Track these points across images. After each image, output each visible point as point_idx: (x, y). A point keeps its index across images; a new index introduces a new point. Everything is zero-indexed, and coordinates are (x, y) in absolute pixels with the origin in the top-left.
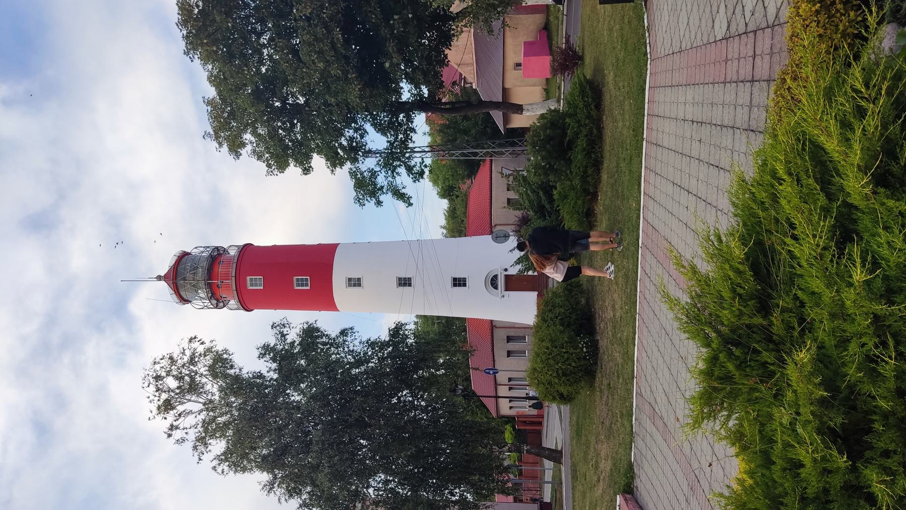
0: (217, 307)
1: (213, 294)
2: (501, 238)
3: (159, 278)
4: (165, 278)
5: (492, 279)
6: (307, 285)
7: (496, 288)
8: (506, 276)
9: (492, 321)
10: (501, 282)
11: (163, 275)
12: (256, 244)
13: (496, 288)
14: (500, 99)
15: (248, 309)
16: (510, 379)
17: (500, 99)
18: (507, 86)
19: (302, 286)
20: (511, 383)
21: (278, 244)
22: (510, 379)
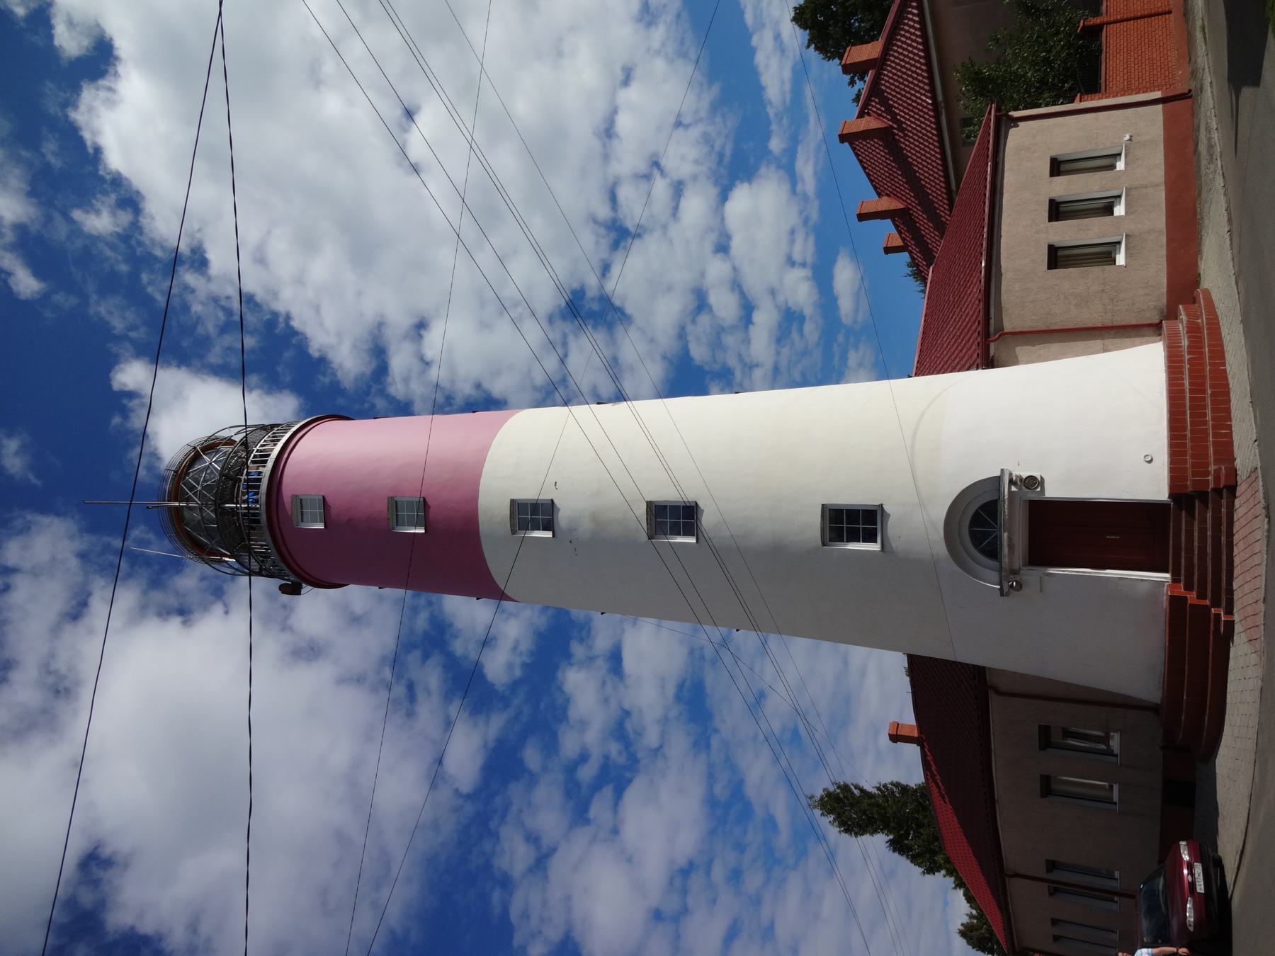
2: (533, 514)
5: (977, 520)
7: (992, 552)
10: (1014, 535)
13: (992, 552)
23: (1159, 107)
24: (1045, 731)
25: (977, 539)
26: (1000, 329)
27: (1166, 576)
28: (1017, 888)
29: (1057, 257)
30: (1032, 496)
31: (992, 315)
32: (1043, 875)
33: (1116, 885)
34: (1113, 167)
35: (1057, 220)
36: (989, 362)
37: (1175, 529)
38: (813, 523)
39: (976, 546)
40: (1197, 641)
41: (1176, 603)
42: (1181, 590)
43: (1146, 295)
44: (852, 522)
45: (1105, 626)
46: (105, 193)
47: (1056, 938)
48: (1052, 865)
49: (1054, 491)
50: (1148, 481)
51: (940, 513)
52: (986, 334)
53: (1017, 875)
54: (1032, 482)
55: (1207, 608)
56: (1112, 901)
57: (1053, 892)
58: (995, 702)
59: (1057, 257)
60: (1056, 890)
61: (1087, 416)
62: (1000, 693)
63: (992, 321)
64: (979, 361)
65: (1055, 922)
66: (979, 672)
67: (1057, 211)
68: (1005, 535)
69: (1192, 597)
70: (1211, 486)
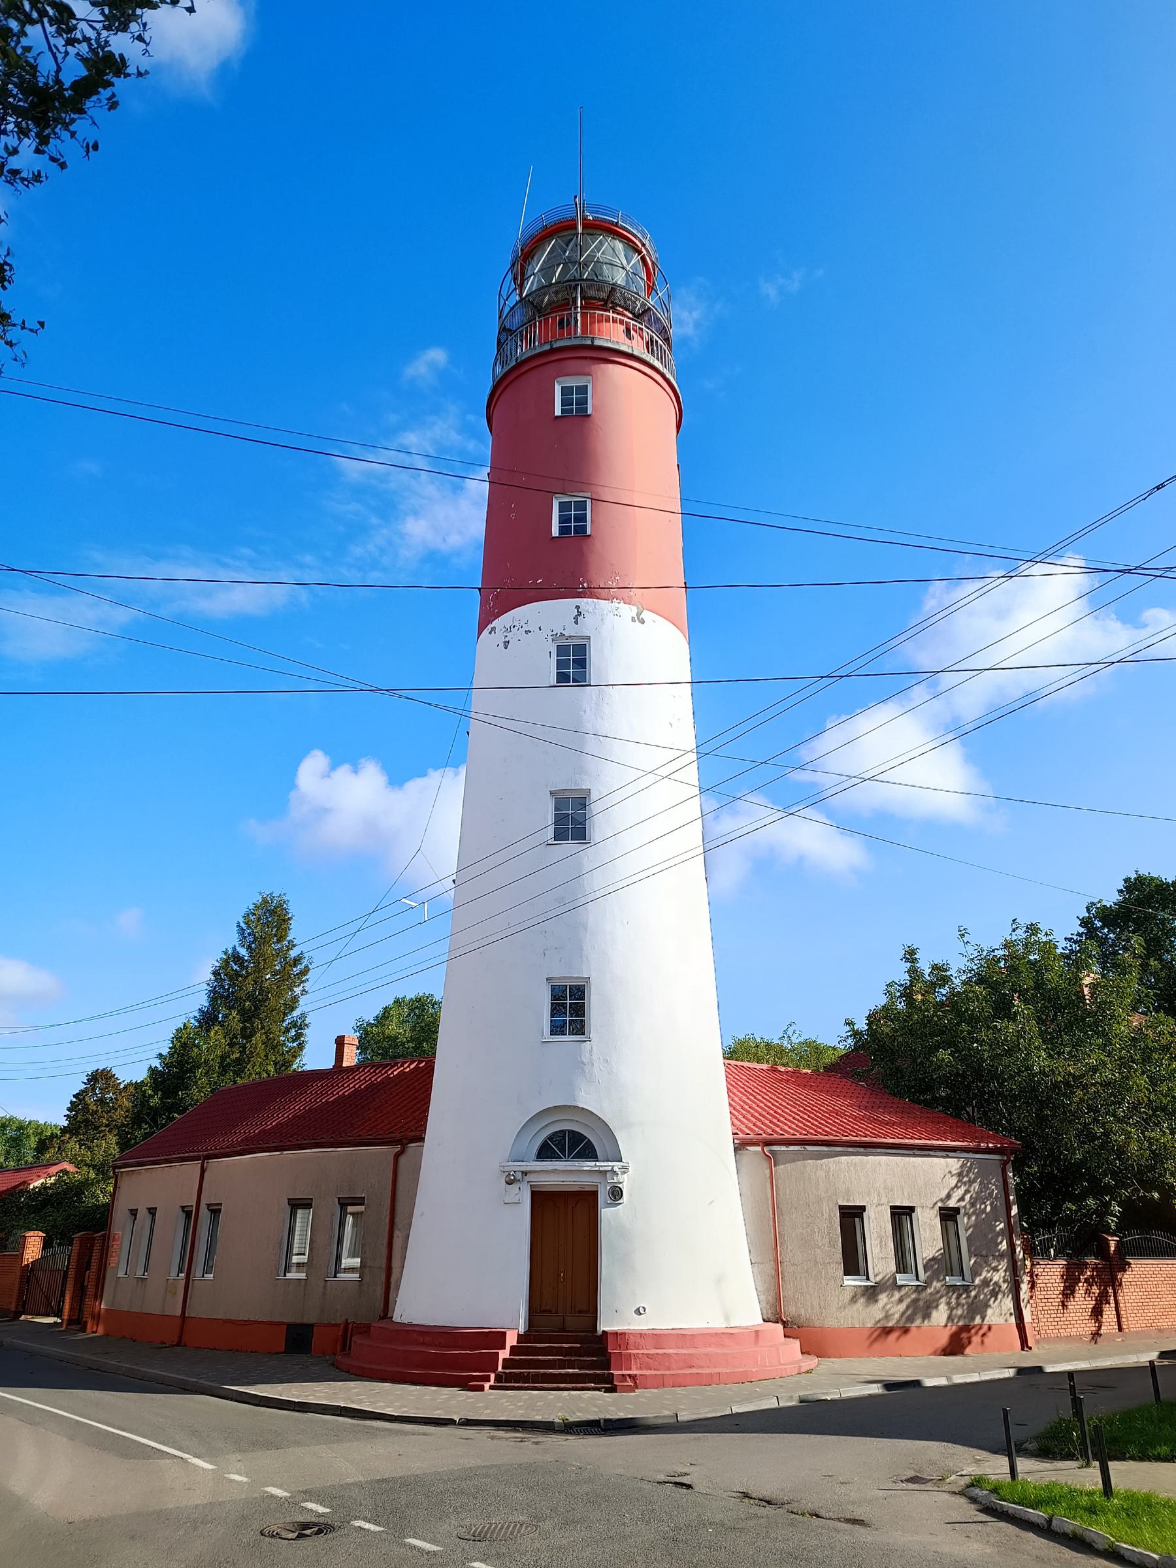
7: (545, 1152)
10: (564, 1174)
13: (545, 1152)
29: (851, 1216)
30: (603, 1197)
31: (792, 1148)
35: (892, 1214)
36: (740, 1146)
37: (568, 1335)
39: (551, 1137)
40: (453, 1357)
43: (812, 1307)
44: (570, 1008)
45: (464, 1262)
47: (134, 1213)
48: (215, 1211)
51: (585, 1100)
53: (203, 1171)
55: (495, 1370)
57: (188, 1214)
60: (188, 1215)
61: (692, 1259)
62: (397, 1156)
63: (783, 1148)
64: (741, 1135)
65: (152, 1211)
67: (901, 1215)
68: (243, 597)
69: (504, 1354)
70: (616, 1373)
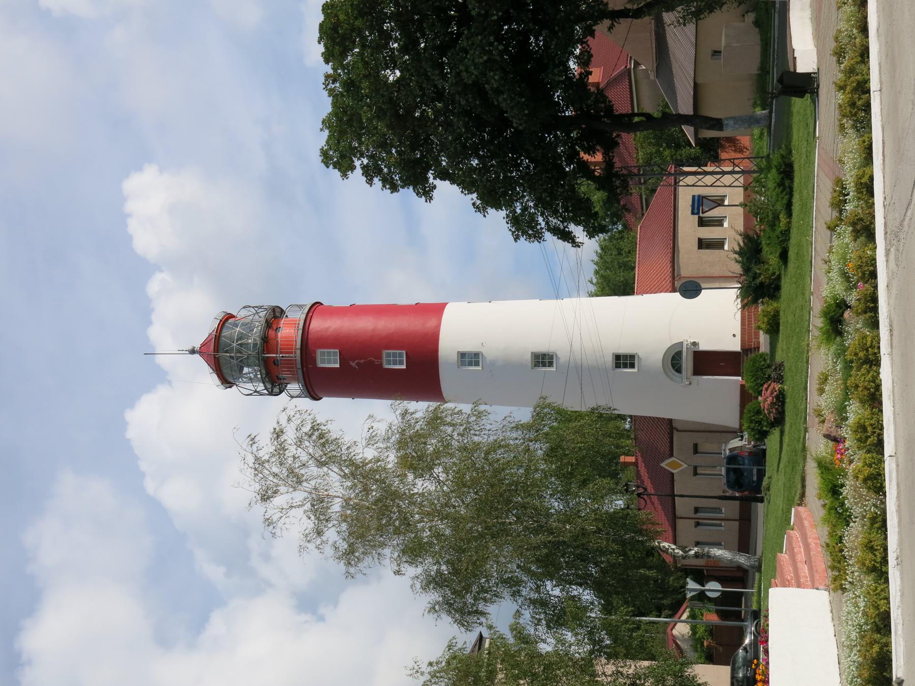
0: (271, 393)
1: (267, 374)
2: (469, 359)
3: (193, 352)
4: (201, 351)
5: (673, 358)
6: (401, 363)
7: (679, 370)
8: (695, 352)
9: (670, 421)
10: (687, 363)
11: (197, 346)
12: (357, 304)
13: (679, 370)
14: (690, 112)
15: (316, 398)
16: (697, 510)
17: (690, 112)
18: (699, 82)
19: (395, 364)
20: (699, 515)
21: (422, 302)
22: (697, 510)
23: (738, 502)
24: (696, 447)
25: (673, 365)
26: (679, 275)
27: (740, 378)
28: (680, 523)
29: (703, 244)
32: (693, 516)
33: (722, 516)
34: (722, 225)
38: (610, 360)
41: (742, 386)
42: (744, 383)
44: (624, 361)
46: (867, 413)
49: (703, 347)
50: (735, 345)
52: (673, 278)
54: (694, 344)
56: (721, 526)
58: (675, 432)
59: (703, 244)
62: (677, 430)
66: (670, 421)
